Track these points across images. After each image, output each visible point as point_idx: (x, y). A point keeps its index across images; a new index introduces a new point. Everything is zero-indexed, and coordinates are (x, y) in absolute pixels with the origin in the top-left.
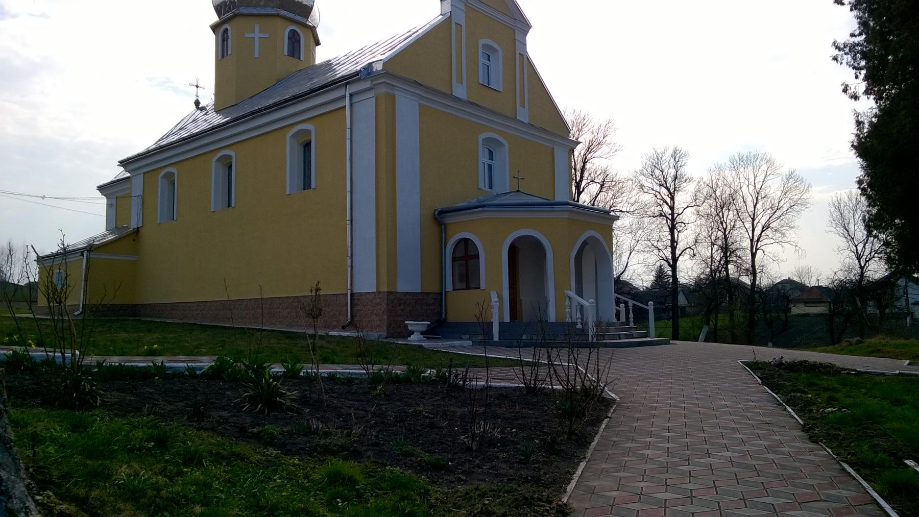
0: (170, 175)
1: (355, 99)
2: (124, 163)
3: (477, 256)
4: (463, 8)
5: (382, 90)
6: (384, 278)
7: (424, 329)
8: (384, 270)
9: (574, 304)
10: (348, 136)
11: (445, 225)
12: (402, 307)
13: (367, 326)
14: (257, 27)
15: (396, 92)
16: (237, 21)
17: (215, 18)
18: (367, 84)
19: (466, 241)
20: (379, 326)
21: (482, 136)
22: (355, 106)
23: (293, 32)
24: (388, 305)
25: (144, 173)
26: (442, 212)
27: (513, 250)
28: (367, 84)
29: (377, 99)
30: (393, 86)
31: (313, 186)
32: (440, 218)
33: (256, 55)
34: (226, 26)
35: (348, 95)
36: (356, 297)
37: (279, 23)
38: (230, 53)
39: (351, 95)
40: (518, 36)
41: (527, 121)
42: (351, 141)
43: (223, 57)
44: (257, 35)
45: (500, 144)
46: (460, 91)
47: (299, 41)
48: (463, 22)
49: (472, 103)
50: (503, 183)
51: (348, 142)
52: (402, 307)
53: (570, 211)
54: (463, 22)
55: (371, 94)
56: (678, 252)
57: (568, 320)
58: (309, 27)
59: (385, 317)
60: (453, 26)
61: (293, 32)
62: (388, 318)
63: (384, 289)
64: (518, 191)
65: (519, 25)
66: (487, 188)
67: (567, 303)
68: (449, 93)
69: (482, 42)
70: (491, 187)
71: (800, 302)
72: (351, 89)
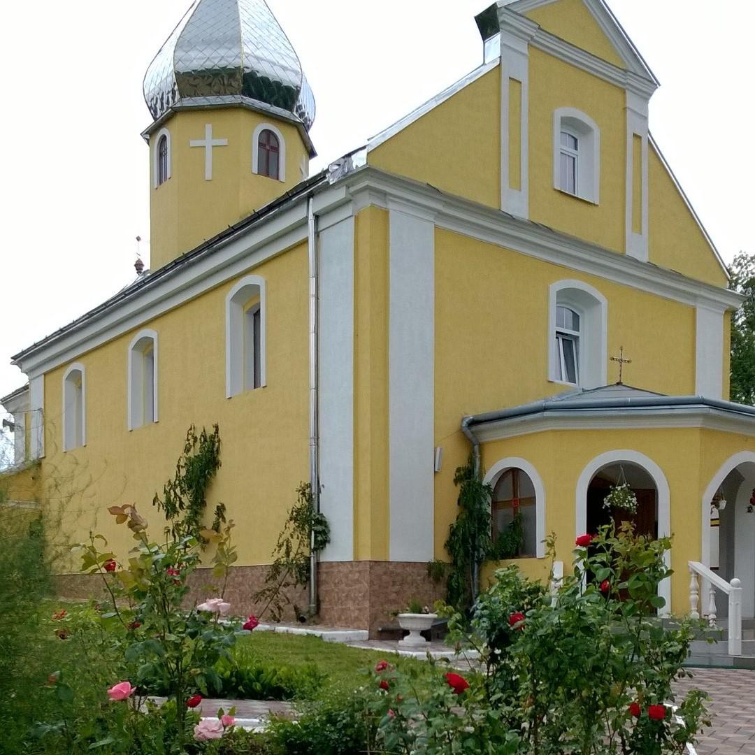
0: (76, 376)
1: (323, 224)
2: (20, 359)
3: (532, 500)
4: (526, 51)
5: (366, 201)
6: (366, 539)
7: (427, 626)
8: (366, 524)
9: (707, 587)
10: (313, 291)
11: (480, 445)
12: (397, 588)
13: (339, 619)
14: (209, 127)
15: (391, 206)
16: (179, 121)
17: (148, 121)
18: (340, 194)
19: (514, 473)
20: (357, 619)
21: (557, 285)
22: (323, 235)
23: (268, 134)
24: (371, 583)
25: (45, 374)
26: (474, 423)
27: (599, 487)
28: (340, 194)
29: (357, 219)
30: (385, 194)
31: (263, 384)
32: (473, 433)
33: (208, 176)
34: (164, 131)
35: (311, 217)
36: (323, 569)
37: (243, 119)
38: (168, 176)
39: (317, 217)
40: (632, 101)
41: (645, 259)
42: (317, 298)
43: (160, 182)
44: (209, 142)
45: (592, 302)
46: (516, 204)
47: (276, 149)
48: (523, 77)
49: (536, 225)
50: (595, 372)
51: (313, 300)
52: (397, 588)
53: (705, 416)
54: (523, 77)
55: (348, 211)
56: (319, 230)
57: (694, 615)
58: (295, 125)
59: (367, 604)
60: (505, 82)
61: (268, 134)
62: (372, 606)
63: (366, 556)
64: (618, 384)
65: (631, 78)
66: (565, 382)
67: (693, 583)
68: (494, 206)
69: (561, 112)
70: (572, 378)
71: (644, 264)
72: (316, 205)
